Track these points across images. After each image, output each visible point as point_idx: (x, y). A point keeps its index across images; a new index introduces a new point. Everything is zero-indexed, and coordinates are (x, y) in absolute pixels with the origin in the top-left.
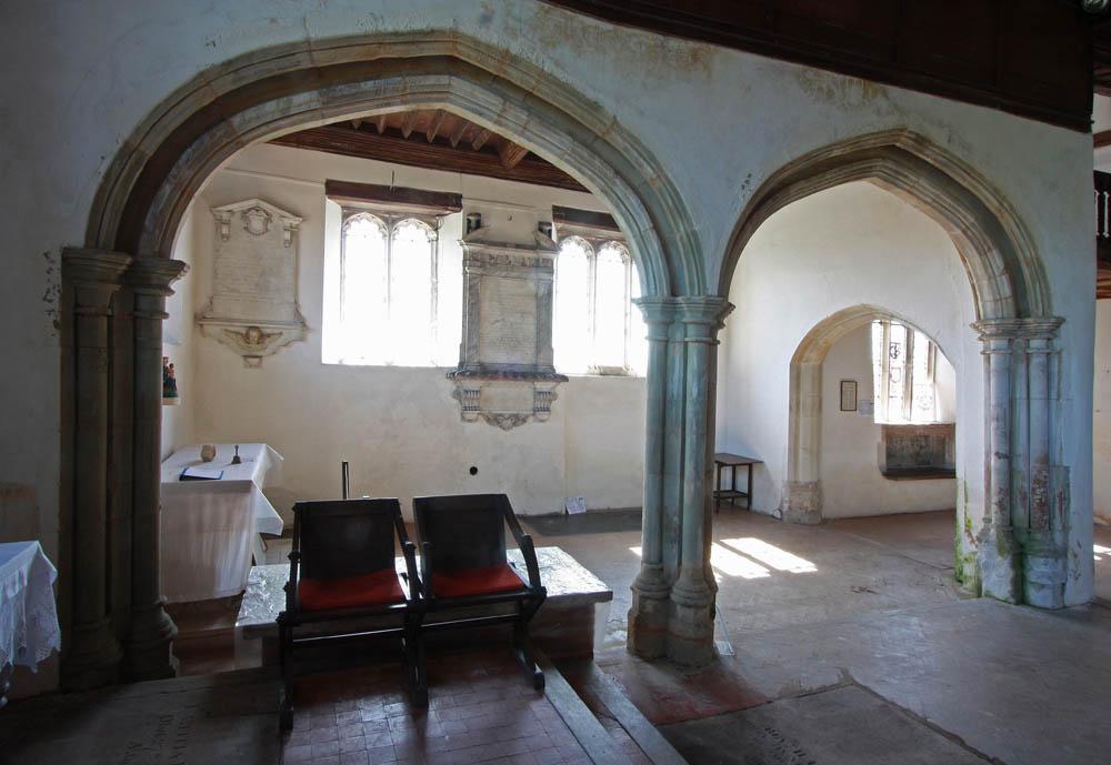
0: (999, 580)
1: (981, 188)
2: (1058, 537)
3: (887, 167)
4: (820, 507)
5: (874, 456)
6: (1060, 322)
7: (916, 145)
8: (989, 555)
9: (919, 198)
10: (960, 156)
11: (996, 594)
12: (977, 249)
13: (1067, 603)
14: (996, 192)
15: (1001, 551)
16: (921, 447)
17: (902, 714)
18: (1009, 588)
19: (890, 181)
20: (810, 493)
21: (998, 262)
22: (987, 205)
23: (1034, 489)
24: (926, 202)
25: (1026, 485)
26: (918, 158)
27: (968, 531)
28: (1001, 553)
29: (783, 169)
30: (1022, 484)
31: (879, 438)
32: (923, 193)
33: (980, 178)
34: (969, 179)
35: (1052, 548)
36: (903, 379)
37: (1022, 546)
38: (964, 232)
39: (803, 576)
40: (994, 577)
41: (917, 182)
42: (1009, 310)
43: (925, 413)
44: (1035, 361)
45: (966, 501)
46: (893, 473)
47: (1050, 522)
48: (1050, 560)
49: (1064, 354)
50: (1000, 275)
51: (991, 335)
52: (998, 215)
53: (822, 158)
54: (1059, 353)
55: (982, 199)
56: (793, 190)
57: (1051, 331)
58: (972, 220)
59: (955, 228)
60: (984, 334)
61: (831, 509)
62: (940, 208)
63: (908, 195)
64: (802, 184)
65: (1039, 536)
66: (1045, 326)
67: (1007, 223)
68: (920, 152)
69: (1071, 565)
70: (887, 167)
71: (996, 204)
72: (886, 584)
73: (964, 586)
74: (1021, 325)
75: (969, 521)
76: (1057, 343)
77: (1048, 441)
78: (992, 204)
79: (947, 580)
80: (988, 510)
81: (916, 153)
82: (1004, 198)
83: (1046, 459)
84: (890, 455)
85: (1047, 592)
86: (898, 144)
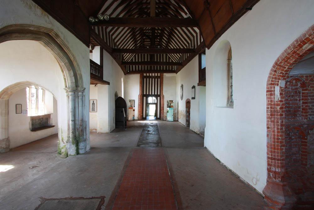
0: (72, 150)
1: (70, 54)
2: (85, 137)
3: (46, 40)
4: (9, 145)
5: (27, 125)
6: (85, 89)
7: (55, 36)
8: (70, 145)
9: (54, 52)
10: (66, 44)
11: (72, 154)
12: (68, 69)
13: (87, 151)
14: (73, 56)
15: (73, 144)
16: (41, 121)
17: (65, 201)
18: (75, 152)
19: (47, 44)
20: (5, 142)
21: (72, 74)
22: (71, 58)
23: (80, 127)
24: (56, 54)
25: (78, 126)
26: (55, 40)
27: (63, 141)
28: (73, 144)
29: (11, 26)
30: (77, 126)
31: (29, 121)
32: (56, 51)
33: (70, 50)
34: (68, 50)
35: (84, 139)
36: (35, 104)
37: (77, 141)
38: (65, 64)
39: (9, 172)
40: (71, 150)
41: (54, 47)
42: (74, 85)
43: (41, 111)
44: (80, 98)
45: (62, 133)
46: (34, 129)
47: (83, 134)
48: (84, 142)
49: (85, 96)
50: (73, 76)
51: (70, 91)
52: (73, 61)
53: (26, 28)
54: (85, 96)
55: (70, 57)
56: (14, 35)
57: (83, 91)
58: (67, 62)
59: (63, 63)
60: (67, 91)
61: (13, 145)
62: (59, 56)
63: (51, 50)
64: (17, 35)
65: (81, 138)
66: (82, 90)
67: (75, 64)
68: (57, 39)
69: (87, 142)
70: (46, 40)
71: (73, 59)
72: (40, 162)
73: (62, 155)
74: (77, 89)
75: (63, 138)
76: (84, 94)
77: (83, 116)
78: (72, 59)
79: (56, 155)
80: (69, 134)
81: (55, 39)
82: (75, 58)
83: (82, 120)
84: (32, 125)
85: (83, 150)
86: (50, 34)
